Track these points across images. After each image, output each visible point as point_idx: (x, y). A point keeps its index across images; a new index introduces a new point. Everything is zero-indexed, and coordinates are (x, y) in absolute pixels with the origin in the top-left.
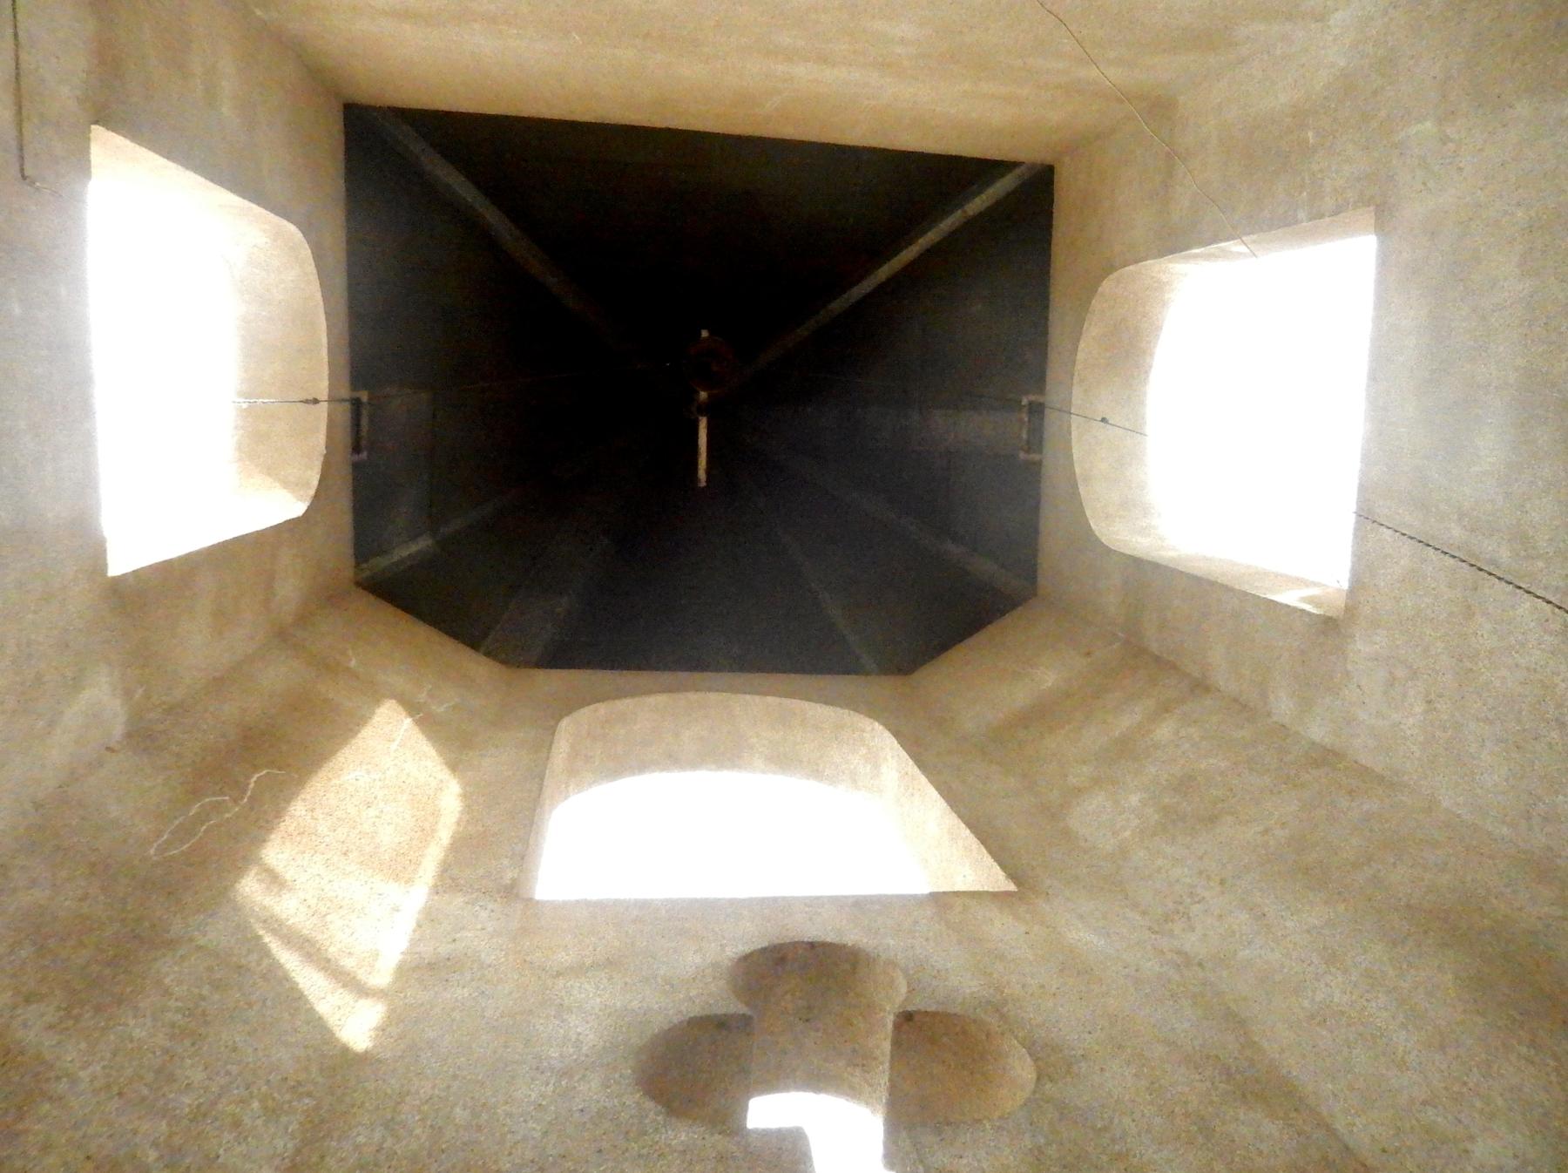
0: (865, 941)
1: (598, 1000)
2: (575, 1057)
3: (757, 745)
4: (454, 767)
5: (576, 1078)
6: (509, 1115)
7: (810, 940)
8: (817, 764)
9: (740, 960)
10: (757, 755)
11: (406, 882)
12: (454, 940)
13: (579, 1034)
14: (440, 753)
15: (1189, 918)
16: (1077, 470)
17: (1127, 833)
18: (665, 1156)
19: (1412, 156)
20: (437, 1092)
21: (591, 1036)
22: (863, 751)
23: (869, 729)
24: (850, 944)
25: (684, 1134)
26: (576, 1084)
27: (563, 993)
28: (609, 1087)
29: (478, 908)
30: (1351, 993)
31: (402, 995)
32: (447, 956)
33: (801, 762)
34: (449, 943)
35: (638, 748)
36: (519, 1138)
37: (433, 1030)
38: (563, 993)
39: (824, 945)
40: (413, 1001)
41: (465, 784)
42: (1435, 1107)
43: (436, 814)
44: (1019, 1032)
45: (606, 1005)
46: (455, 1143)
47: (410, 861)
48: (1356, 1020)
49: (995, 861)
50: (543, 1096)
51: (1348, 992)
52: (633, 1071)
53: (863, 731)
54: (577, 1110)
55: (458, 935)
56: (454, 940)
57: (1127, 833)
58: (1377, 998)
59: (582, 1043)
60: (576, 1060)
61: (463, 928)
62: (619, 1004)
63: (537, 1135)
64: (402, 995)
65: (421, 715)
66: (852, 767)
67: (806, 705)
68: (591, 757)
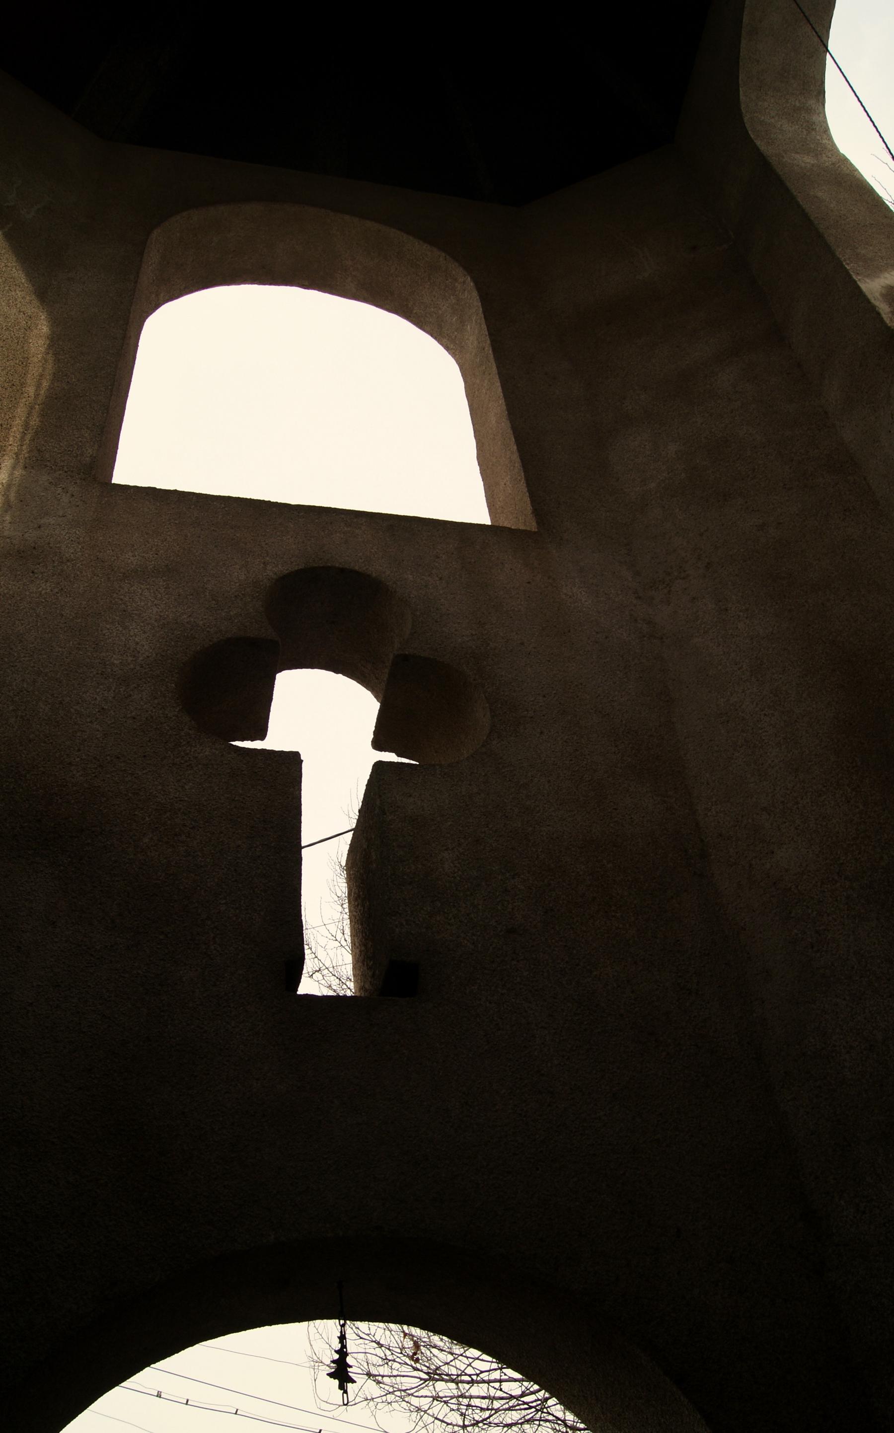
0: (388, 573)
1: (155, 609)
4: (42, 294)
7: (341, 566)
10: (350, 279)
13: (137, 643)
14: (30, 277)
15: (669, 592)
16: (746, 19)
17: (653, 485)
19: (746, 502)
21: (146, 647)
23: (461, 280)
26: (131, 693)
27: (127, 599)
29: (60, 490)
30: (757, 704)
32: (33, 545)
38: (127, 599)
40: (6, 591)
41: (54, 322)
43: (25, 362)
44: (489, 688)
45: (161, 616)
49: (529, 491)
51: (755, 703)
52: (176, 685)
53: (456, 280)
57: (653, 485)
58: (773, 715)
66: (440, 312)
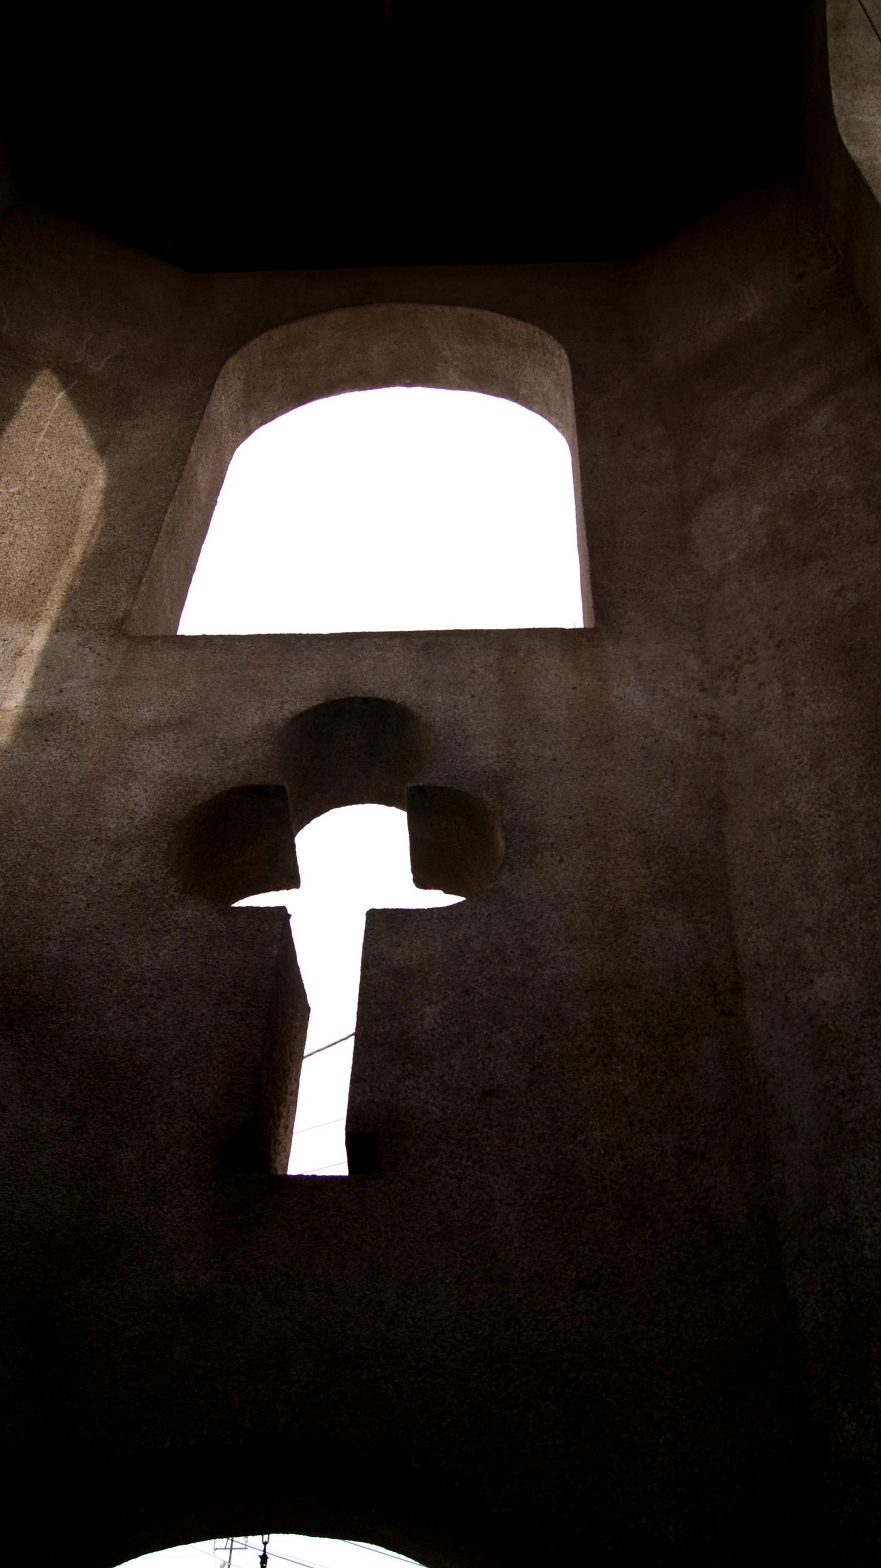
0: (415, 696)
1: (161, 766)
2: (127, 829)
3: (451, 359)
5: (123, 851)
6: (66, 885)
7: (364, 696)
8: (512, 382)
9: (293, 720)
10: (451, 370)
11: (33, 618)
12: (61, 692)
13: (136, 804)
18: (170, 933)
20: (19, 860)
22: (554, 376)
24: (399, 701)
25: (190, 911)
28: (146, 861)
31: (9, 755)
33: (497, 378)
34: (56, 694)
35: (323, 368)
36: (69, 908)
37: (26, 796)
39: (377, 700)
41: (112, 474)
42: (813, 936)
46: (252, 646)
47: (40, 591)
48: (802, 834)
50: (95, 868)
53: (553, 354)
54: (116, 884)
55: (64, 686)
56: (61, 692)
59: (136, 813)
60: (127, 832)
61: (70, 677)
62: (176, 771)
63: (82, 905)
64: (9, 755)
65: (77, 381)
66: (545, 390)
67: (498, 318)
68: (271, 386)
